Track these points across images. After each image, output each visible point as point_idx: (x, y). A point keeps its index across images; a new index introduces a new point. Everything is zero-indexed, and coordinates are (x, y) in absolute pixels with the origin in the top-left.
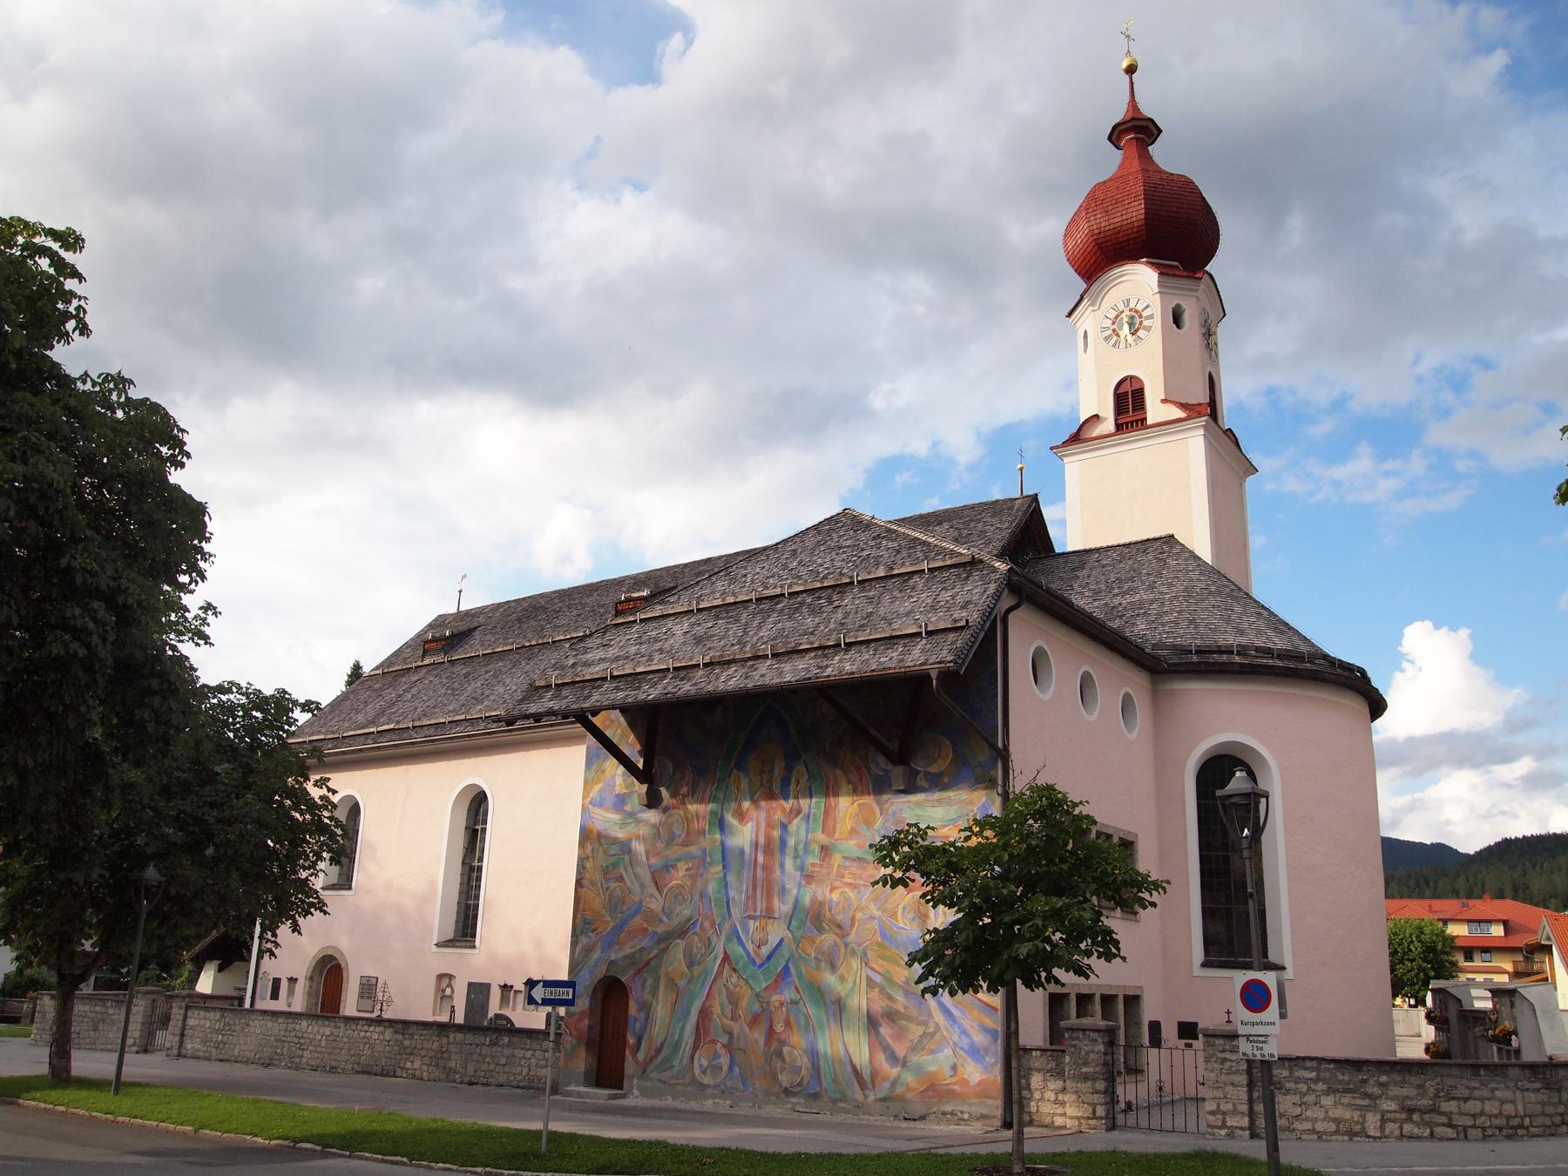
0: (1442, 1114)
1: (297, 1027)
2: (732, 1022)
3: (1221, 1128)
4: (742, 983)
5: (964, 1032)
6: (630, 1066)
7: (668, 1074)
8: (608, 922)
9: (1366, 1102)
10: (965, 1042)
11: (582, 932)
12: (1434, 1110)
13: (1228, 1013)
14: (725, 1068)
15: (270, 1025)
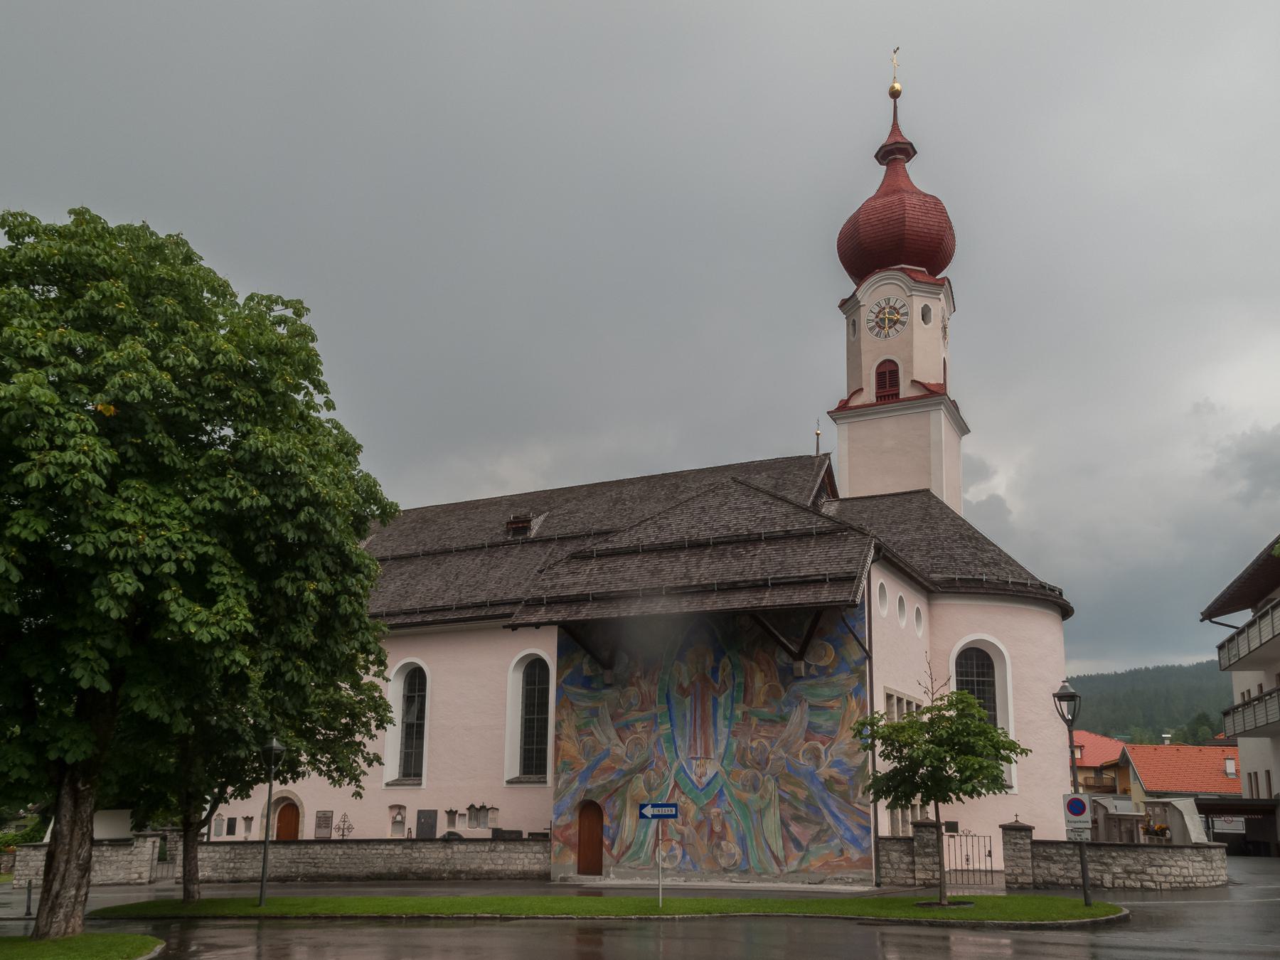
0: (1148, 874)
1: (310, 851)
2: (683, 827)
3: (1014, 883)
4: (689, 801)
5: (848, 829)
6: (607, 859)
7: (637, 862)
8: (583, 764)
9: (1105, 867)
10: (848, 835)
11: (563, 771)
12: (1143, 872)
13: (1016, 816)
14: (679, 857)
15: (282, 851)
